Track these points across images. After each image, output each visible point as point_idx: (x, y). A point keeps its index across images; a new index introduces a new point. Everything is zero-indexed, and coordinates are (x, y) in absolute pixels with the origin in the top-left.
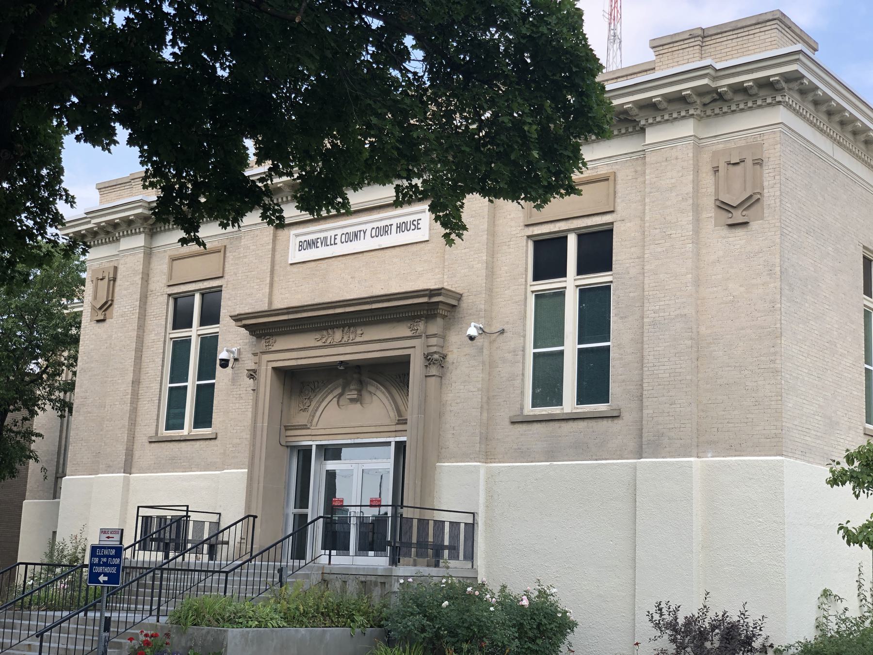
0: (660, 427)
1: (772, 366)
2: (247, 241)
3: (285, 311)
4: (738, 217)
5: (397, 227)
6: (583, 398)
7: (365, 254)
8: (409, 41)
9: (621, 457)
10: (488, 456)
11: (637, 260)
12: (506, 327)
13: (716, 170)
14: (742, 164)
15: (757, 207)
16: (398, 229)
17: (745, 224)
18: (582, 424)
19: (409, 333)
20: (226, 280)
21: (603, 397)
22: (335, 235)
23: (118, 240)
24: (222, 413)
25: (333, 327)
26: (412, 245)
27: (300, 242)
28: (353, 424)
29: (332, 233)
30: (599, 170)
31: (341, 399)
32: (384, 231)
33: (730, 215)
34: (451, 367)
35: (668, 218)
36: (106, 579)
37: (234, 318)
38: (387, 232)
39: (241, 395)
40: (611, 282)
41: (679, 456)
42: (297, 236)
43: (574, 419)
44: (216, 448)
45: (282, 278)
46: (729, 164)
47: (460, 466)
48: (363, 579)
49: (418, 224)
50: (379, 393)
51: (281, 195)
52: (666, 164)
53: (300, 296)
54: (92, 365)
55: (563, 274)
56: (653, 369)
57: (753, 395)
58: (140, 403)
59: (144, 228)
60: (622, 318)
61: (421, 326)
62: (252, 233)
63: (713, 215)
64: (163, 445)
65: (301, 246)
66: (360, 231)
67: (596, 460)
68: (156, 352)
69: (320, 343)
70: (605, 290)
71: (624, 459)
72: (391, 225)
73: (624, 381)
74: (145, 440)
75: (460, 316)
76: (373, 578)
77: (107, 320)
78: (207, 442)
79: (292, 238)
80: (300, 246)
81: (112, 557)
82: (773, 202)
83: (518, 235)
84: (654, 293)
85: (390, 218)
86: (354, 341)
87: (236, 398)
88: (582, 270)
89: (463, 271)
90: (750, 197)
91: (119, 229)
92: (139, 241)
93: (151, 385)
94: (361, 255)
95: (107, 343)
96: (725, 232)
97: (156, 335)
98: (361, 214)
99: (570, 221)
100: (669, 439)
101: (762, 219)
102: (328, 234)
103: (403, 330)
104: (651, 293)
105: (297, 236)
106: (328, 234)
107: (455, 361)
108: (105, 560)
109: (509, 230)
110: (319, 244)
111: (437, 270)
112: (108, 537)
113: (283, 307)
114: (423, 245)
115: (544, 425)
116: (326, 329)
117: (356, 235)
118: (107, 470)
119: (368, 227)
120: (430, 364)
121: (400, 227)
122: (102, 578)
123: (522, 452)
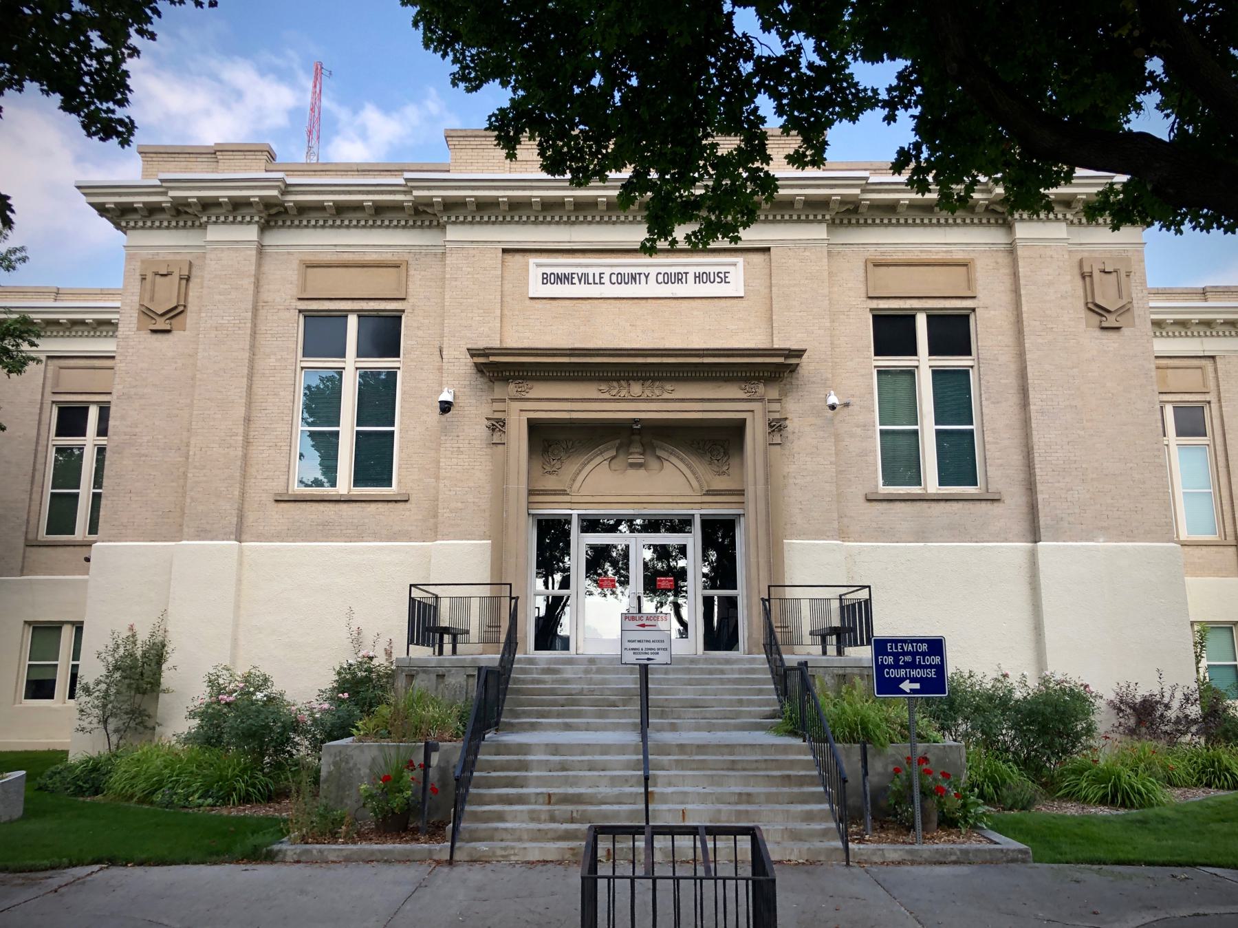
0: (1058, 512)
1: (1157, 460)
2: (457, 260)
3: (568, 352)
4: (161, 324)
5: (696, 277)
7: (649, 301)
8: (1146, 74)
9: (1006, 540)
10: (843, 535)
11: (1006, 348)
12: (852, 400)
13: (143, 279)
14: (169, 276)
15: (1127, 315)
16: (697, 279)
17: (1118, 328)
18: (955, 506)
19: (741, 395)
20: (411, 304)
22: (600, 274)
23: (203, 226)
24: (417, 470)
25: (628, 379)
26: (719, 300)
27: (543, 274)
28: (634, 492)
29: (597, 271)
30: (954, 254)
31: (613, 461)
32: (679, 278)
33: (154, 322)
34: (791, 437)
35: (1048, 312)
36: (917, 686)
37: (471, 352)
38: (681, 280)
39: (461, 449)
40: (399, 368)
41: (1081, 540)
43: (947, 500)
44: (408, 513)
45: (517, 313)
46: (157, 274)
47: (817, 544)
48: (841, 672)
49: (726, 277)
50: (673, 459)
51: (520, 213)
52: (1040, 260)
54: (145, 391)
55: (342, 354)
56: (1045, 455)
57: (1142, 486)
58: (251, 448)
59: (261, 218)
60: (993, 403)
61: (761, 389)
62: (463, 252)
63: (1083, 316)
64: (303, 505)
65: (546, 278)
66: (640, 274)
67: (977, 542)
68: (282, 382)
69: (607, 396)
71: (1010, 542)
72: (686, 273)
73: (1001, 465)
74: (268, 499)
75: (799, 383)
76: (856, 671)
77: (174, 332)
78: (391, 505)
79: (532, 267)
80: (543, 278)
81: (924, 654)
82: (1142, 313)
83: (860, 306)
84: (1039, 382)
85: (648, 266)
86: (660, 397)
87: (452, 452)
89: (799, 335)
90: (1124, 306)
91: (344, 216)
92: (250, 233)
93: (272, 426)
94: (644, 301)
95: (176, 363)
96: (1098, 333)
97: (277, 360)
98: (726, 254)
99: (924, 300)
100: (1069, 524)
101: (1134, 326)
102: (590, 271)
104: (1036, 382)
105: (538, 265)
106: (590, 271)
107: (797, 431)
109: (846, 299)
111: (757, 330)
112: (643, 626)
113: (567, 347)
114: (736, 301)
115: (909, 503)
117: (633, 278)
118: (199, 536)
119: (653, 272)
120: (774, 431)
121: (699, 277)
123: (884, 531)
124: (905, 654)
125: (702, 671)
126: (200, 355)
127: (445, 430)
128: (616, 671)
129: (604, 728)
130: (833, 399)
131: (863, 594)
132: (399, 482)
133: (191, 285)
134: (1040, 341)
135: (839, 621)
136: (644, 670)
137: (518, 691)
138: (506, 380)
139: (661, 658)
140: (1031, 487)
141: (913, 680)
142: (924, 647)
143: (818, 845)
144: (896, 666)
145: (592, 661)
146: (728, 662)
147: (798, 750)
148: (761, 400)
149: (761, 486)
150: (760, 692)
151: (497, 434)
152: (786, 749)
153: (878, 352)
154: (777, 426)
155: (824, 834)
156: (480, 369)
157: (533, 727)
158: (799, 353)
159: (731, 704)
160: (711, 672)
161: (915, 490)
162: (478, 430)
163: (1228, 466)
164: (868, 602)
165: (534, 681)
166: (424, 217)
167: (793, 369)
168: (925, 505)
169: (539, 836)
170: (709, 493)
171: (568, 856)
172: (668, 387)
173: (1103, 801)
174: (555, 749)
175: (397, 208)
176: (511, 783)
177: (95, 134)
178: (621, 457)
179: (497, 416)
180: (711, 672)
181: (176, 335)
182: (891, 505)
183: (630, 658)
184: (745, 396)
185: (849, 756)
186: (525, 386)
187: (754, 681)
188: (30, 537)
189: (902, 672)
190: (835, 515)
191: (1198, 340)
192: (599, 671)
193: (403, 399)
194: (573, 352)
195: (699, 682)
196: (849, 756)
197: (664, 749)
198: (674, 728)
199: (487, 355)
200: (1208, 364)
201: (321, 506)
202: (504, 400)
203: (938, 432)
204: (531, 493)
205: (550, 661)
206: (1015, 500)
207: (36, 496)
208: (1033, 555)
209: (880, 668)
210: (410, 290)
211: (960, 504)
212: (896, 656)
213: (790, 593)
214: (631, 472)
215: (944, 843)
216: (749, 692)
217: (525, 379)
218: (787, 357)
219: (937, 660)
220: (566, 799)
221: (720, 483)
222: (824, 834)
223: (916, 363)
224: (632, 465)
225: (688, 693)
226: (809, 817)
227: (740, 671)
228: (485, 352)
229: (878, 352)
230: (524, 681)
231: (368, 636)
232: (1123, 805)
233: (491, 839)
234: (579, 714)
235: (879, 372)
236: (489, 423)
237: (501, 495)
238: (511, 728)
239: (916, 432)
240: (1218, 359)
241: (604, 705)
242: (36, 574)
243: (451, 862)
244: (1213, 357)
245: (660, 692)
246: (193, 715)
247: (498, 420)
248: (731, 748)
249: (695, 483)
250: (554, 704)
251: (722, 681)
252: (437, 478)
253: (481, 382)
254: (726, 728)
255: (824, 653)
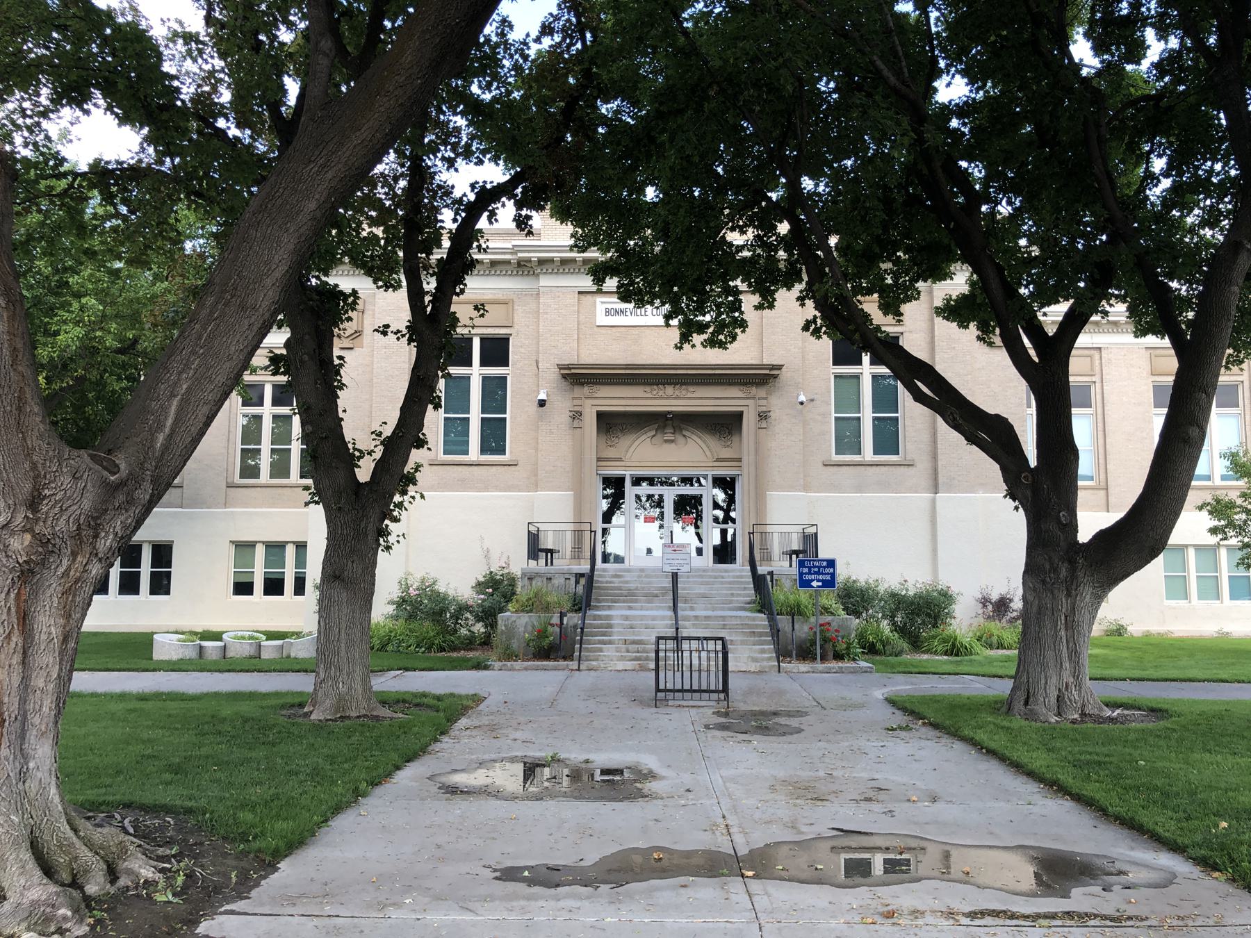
6: (484, 449)
9: (916, 492)
10: (806, 488)
12: (815, 397)
21: (502, 451)
25: (664, 384)
36: (820, 584)
41: (966, 492)
42: (603, 303)
50: (694, 437)
53: (610, 354)
64: (448, 467)
70: (502, 380)
81: (824, 567)
88: (484, 363)
103: (734, 392)
105: (603, 303)
108: (816, 570)
110: (628, 313)
116: (653, 384)
122: (815, 584)
124: (814, 567)
125: (710, 577)
126: (375, 366)
127: (541, 418)
128: (657, 576)
129: (652, 609)
130: (802, 398)
131: (812, 530)
132: (511, 452)
133: (365, 316)
134: (946, 356)
135: (78, 690)
136: (675, 576)
137: (599, 588)
138: (582, 384)
139: (686, 568)
140: (934, 457)
141: (818, 581)
142: (825, 564)
143: (765, 663)
144: (810, 573)
145: (642, 570)
146: (726, 571)
147: (762, 620)
148: (754, 398)
149: (752, 457)
150: (745, 589)
151: (576, 421)
152: (754, 619)
153: (836, 363)
154: (763, 416)
155: (769, 659)
156: (564, 377)
157: (609, 608)
158: (779, 367)
159: (726, 595)
160: (716, 577)
161: (856, 458)
162: (565, 417)
163: (1104, 431)
164: (816, 534)
165: (607, 582)
166: (525, 269)
167: (775, 377)
168: (863, 468)
169: (622, 659)
170: (718, 460)
171: (637, 667)
172: (691, 389)
173: (946, 653)
174: (627, 618)
175: (508, 262)
176: (604, 634)
177: (381, 287)
178: (659, 435)
179: (577, 409)
180: (716, 577)
181: (357, 351)
182: (840, 468)
183: (668, 569)
184: (743, 396)
185: (784, 622)
186: (595, 388)
187: (742, 583)
188: (229, 480)
189: (813, 577)
190: (802, 476)
191: (1089, 335)
192: (646, 576)
193: (512, 397)
194: (627, 367)
195: (707, 583)
196: (784, 622)
197: (686, 619)
198: (692, 609)
199: (570, 369)
200: (1096, 354)
201: (460, 468)
202: (581, 398)
203: (875, 419)
204: (599, 460)
205: (616, 570)
206: (923, 465)
207: (231, 451)
208: (934, 501)
209: (801, 574)
210: (515, 320)
211: (887, 468)
212: (810, 568)
213: (769, 529)
214: (667, 446)
215: (835, 665)
216: (739, 589)
217: (595, 383)
218: (771, 369)
219: (832, 570)
220: (634, 642)
221: (726, 453)
222: (769, 659)
223: (860, 371)
224: (666, 441)
225: (701, 590)
226: (763, 651)
227: (734, 577)
228: (568, 367)
229: (836, 363)
230: (601, 582)
231: (495, 555)
232: (957, 655)
233: (597, 660)
234: (636, 601)
235: (836, 377)
236: (571, 414)
237: (579, 461)
238: (597, 608)
239: (859, 419)
240: (1103, 351)
241: (652, 596)
242: (235, 507)
243: (579, 670)
244: (1100, 348)
245: (684, 589)
246: (391, 602)
247: (577, 412)
248: (723, 618)
249: (708, 453)
250: (621, 595)
251: (722, 583)
252: (536, 449)
253: (565, 384)
254: (723, 609)
255: (791, 566)
